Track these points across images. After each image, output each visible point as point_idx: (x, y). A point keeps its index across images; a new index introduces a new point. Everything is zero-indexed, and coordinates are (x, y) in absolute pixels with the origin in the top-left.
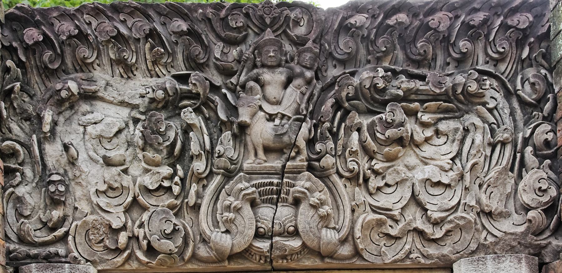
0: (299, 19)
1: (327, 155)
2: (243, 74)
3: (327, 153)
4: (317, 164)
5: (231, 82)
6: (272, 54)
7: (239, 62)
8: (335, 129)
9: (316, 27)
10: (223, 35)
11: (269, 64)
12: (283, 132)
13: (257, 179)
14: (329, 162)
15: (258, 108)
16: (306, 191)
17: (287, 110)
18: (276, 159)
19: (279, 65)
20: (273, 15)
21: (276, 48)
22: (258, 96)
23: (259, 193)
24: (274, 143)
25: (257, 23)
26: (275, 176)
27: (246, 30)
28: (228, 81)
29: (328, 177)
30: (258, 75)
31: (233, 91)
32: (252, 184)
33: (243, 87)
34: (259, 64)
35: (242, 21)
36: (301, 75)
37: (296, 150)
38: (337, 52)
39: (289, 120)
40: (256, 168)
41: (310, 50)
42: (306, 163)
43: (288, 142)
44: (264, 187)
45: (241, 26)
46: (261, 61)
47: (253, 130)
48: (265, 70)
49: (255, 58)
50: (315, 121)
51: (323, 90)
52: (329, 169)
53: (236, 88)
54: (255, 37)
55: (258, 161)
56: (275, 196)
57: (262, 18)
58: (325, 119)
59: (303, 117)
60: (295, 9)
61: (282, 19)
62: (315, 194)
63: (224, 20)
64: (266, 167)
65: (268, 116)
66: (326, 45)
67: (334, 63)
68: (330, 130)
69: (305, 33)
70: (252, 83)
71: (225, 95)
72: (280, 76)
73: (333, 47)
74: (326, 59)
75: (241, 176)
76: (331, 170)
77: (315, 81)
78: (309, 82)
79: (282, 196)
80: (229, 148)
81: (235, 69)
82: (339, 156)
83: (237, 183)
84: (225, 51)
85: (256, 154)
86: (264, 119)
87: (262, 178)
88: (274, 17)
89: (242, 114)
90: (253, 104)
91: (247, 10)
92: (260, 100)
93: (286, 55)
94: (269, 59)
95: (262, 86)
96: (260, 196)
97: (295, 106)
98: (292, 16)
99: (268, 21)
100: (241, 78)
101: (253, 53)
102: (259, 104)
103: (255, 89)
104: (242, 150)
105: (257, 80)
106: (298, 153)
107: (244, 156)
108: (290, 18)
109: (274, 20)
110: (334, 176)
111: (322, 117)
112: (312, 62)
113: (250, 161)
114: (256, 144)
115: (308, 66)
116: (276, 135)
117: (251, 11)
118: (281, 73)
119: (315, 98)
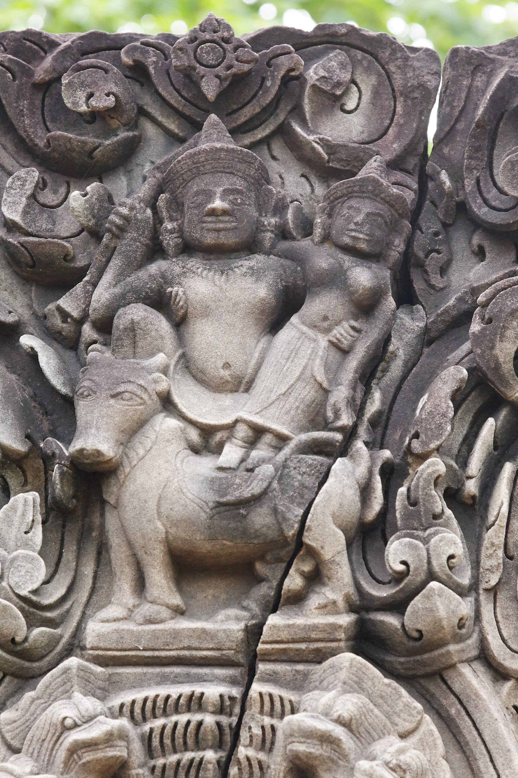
0: (338, 84)
1: (434, 585)
2: (108, 277)
3: (432, 576)
4: (391, 620)
5: (59, 309)
6: (218, 204)
7: (96, 235)
8: (472, 487)
9: (406, 114)
10: (41, 143)
11: (209, 239)
12: (247, 493)
13: (139, 683)
14: (442, 612)
15: (155, 402)
16: (339, 732)
17: (272, 410)
18: (227, 605)
19: (250, 246)
20: (229, 67)
21: (240, 184)
22: (160, 358)
23: (147, 740)
24: (212, 538)
25: (173, 99)
26: (219, 672)
27: (133, 125)
28: (51, 306)
29: (441, 674)
30: (166, 280)
31: (68, 343)
32: (116, 702)
33: (105, 326)
34: (170, 241)
35: (115, 89)
36: (335, 279)
37: (307, 568)
38: (486, 201)
39: (278, 449)
40: (138, 637)
41: (371, 190)
42: (346, 620)
43: (272, 534)
44: (165, 713)
45: (108, 110)
46: (180, 231)
47: (131, 487)
48: (194, 263)
49: (158, 220)
50: (387, 454)
51: (428, 338)
52: (442, 643)
53: (79, 333)
54: (168, 148)
55: (147, 609)
56: (210, 755)
57: (190, 78)
58: (425, 444)
59: (338, 437)
60: (325, 52)
61: (273, 86)
62: (378, 747)
63: (49, 87)
64: (176, 634)
65: (194, 435)
66: (444, 176)
67: (476, 240)
68: (453, 496)
69: (364, 137)
70: (137, 312)
71: (33, 356)
72: (249, 285)
73: (469, 184)
74: (445, 226)
75: (67, 670)
76: (452, 648)
77: (390, 302)
78: (365, 307)
79: (242, 752)
80: (26, 558)
81: (81, 263)
82: (493, 591)
83: (50, 698)
84: (48, 197)
85: (140, 584)
86: (177, 447)
87: (164, 680)
88: (234, 75)
89: (88, 426)
90: (130, 387)
91: (138, 56)
92: (165, 371)
93: (280, 208)
94: (210, 223)
95: (180, 323)
96: (150, 752)
97: (307, 393)
98: (313, 74)
99: (210, 89)
100: (97, 292)
101: (152, 203)
102: (163, 386)
103: (146, 333)
104: (88, 570)
105: (160, 301)
106: (316, 578)
107: (93, 590)
108: (301, 79)
109: (236, 88)
110: (466, 670)
111: (416, 436)
112: (378, 233)
113: (113, 611)
114: (138, 542)
115: (363, 246)
116: (219, 504)
117: (151, 59)
118: (256, 273)
119: (396, 368)
